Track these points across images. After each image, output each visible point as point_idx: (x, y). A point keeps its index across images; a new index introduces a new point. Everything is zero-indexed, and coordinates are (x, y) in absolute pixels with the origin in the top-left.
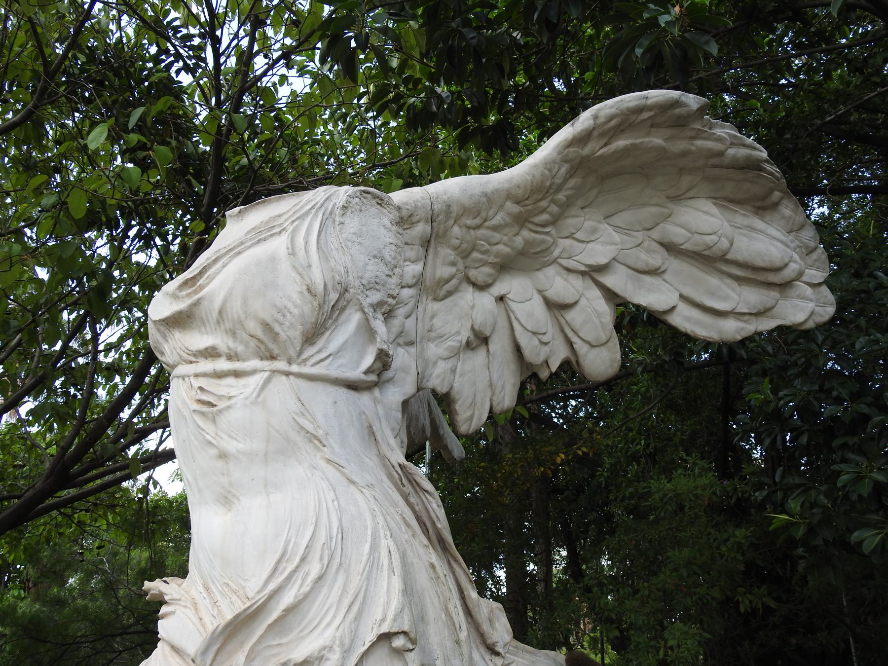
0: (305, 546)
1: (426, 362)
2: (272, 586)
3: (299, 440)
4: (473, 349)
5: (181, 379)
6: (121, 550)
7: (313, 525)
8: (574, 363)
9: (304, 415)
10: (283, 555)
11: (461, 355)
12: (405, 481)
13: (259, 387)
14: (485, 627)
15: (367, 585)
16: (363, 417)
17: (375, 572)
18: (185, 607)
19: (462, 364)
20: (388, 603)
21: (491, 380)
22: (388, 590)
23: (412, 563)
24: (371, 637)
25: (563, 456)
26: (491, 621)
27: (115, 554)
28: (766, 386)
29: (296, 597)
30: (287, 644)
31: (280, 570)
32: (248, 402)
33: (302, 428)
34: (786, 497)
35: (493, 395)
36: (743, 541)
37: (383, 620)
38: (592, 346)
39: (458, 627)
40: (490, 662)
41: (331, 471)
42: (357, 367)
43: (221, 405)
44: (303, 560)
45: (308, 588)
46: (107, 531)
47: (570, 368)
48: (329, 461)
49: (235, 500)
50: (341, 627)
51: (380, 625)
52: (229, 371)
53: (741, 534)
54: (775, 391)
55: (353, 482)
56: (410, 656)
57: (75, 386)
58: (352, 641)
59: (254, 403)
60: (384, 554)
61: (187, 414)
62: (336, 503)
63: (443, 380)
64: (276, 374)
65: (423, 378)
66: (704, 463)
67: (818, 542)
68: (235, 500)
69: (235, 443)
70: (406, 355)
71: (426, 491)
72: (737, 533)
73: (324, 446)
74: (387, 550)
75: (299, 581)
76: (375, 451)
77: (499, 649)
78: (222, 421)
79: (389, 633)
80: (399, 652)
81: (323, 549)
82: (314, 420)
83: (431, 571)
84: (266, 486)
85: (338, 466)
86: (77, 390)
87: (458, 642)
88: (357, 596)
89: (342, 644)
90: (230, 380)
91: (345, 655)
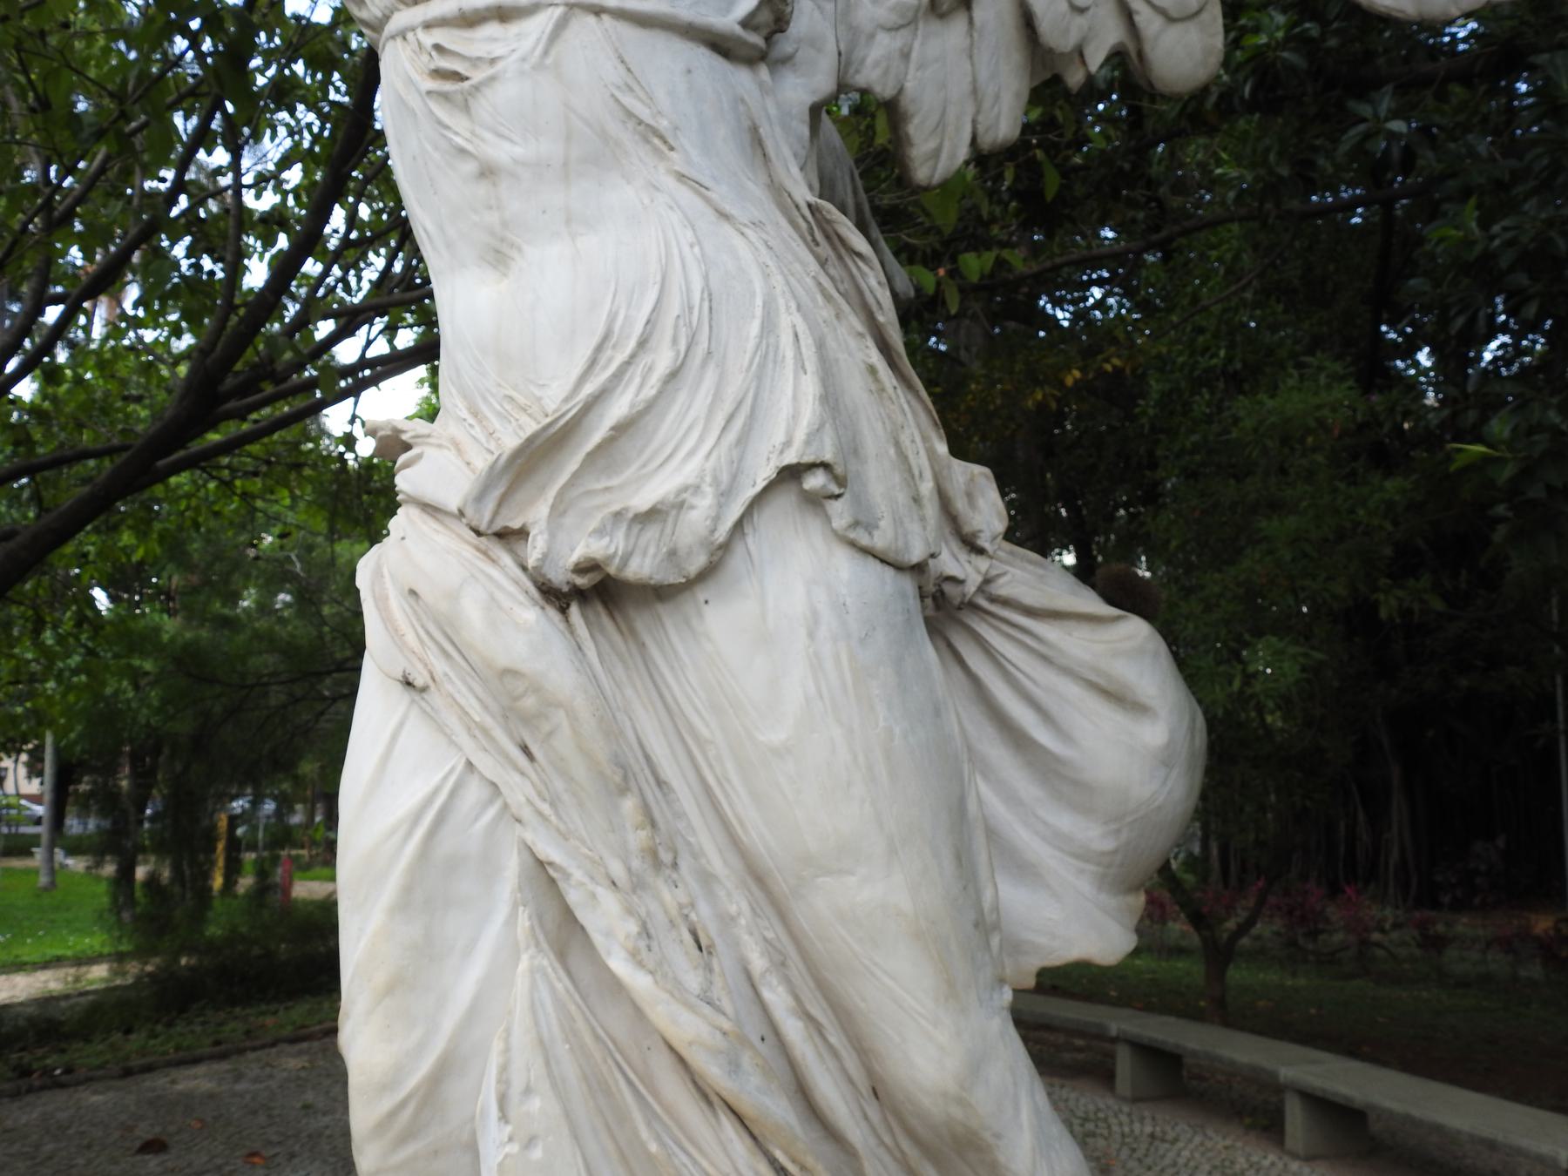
0: (644, 321)
1: (854, 31)
2: (589, 388)
3: (626, 136)
4: (942, 16)
5: (399, 40)
6: (320, 539)
7: (657, 287)
8: (1133, 55)
9: (631, 90)
10: (606, 337)
11: (921, 25)
12: (819, 236)
13: (545, 37)
14: (960, 505)
15: (758, 388)
16: (741, 108)
17: (770, 365)
18: (440, 446)
19: (922, 44)
20: (795, 417)
21: (974, 81)
22: (795, 398)
23: (837, 360)
24: (764, 473)
25: (1077, 374)
26: (970, 496)
27: (310, 548)
28: (1470, 215)
29: (632, 406)
30: (621, 487)
31: (603, 360)
32: (527, 66)
33: (630, 114)
34: (1484, 420)
35: (978, 112)
36: (1397, 498)
37: (788, 444)
38: (1171, 19)
39: (916, 473)
40: (967, 565)
41: (685, 194)
42: (728, 10)
43: (477, 76)
44: (642, 344)
45: (653, 392)
46: (292, 508)
47: (1127, 68)
48: (681, 177)
49: (514, 253)
50: (715, 455)
51: (782, 452)
52: (488, 9)
53: (1393, 486)
54: (1485, 224)
55: (724, 216)
56: (835, 507)
57: (210, 252)
58: (734, 477)
59: (539, 67)
60: (786, 340)
61: (414, 102)
62: (696, 249)
63: (886, 72)
64: (576, 10)
65: (848, 64)
66: (1338, 367)
67: (1536, 492)
68: (514, 253)
69: (507, 145)
70: (817, 14)
71: (859, 255)
72: (1389, 484)
73: (672, 149)
74: (790, 332)
75: (637, 380)
76: (763, 178)
77: (983, 542)
78: (482, 106)
79: (798, 464)
80: (816, 502)
81: (676, 327)
82: (650, 99)
83: (870, 379)
84: (568, 221)
85: (698, 187)
86: (215, 261)
87: (917, 500)
88: (740, 403)
89: (716, 481)
90: (492, 29)
91: (722, 500)
